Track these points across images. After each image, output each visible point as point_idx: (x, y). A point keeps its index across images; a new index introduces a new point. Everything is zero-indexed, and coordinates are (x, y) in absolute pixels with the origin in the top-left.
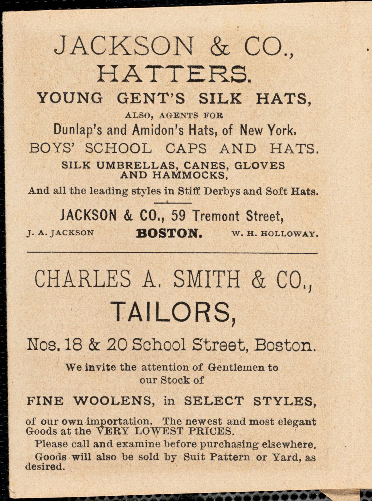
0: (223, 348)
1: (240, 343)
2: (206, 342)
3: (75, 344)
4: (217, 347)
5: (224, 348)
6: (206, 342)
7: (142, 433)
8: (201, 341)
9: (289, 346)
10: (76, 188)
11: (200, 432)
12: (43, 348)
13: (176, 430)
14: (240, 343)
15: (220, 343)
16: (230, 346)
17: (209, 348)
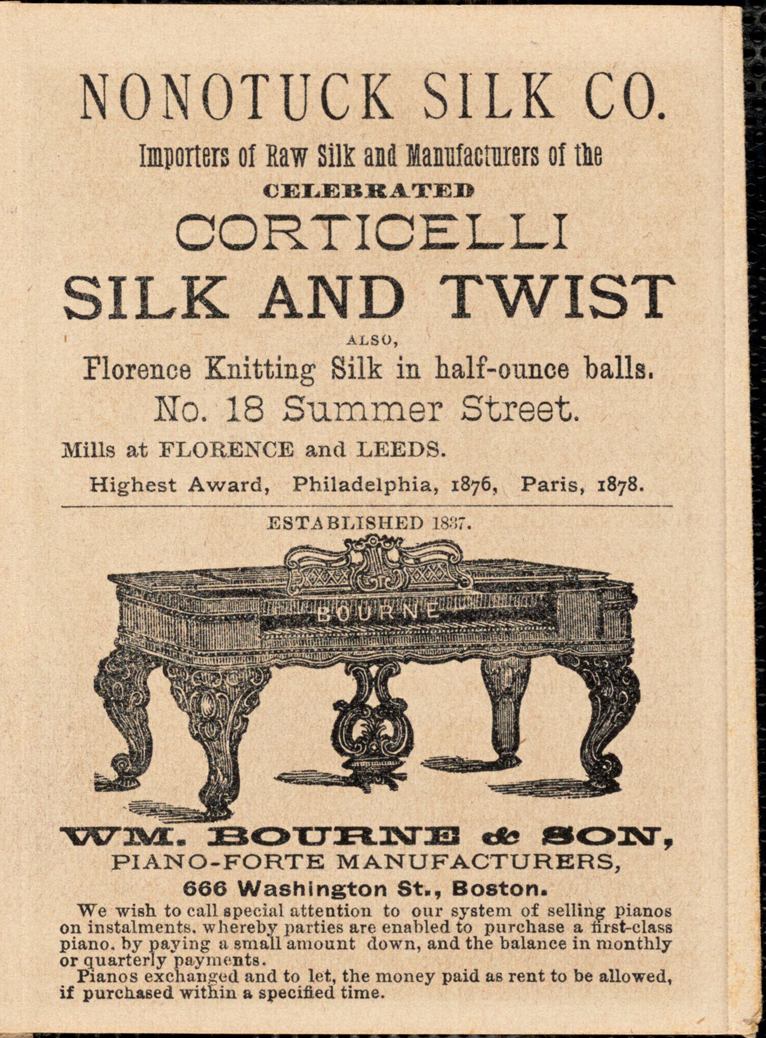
0: (526, 416)
1: (561, 404)
2: (490, 404)
3: (249, 408)
4: (514, 412)
5: (529, 416)
6: (490, 404)
7: (192, 453)
8: (301, 401)
9: (496, 411)
10: (352, 970)
11: (218, 453)
12: (188, 416)
13: (293, 522)
14: (561, 404)
15: (519, 405)
16: (539, 411)
17: (498, 417)
